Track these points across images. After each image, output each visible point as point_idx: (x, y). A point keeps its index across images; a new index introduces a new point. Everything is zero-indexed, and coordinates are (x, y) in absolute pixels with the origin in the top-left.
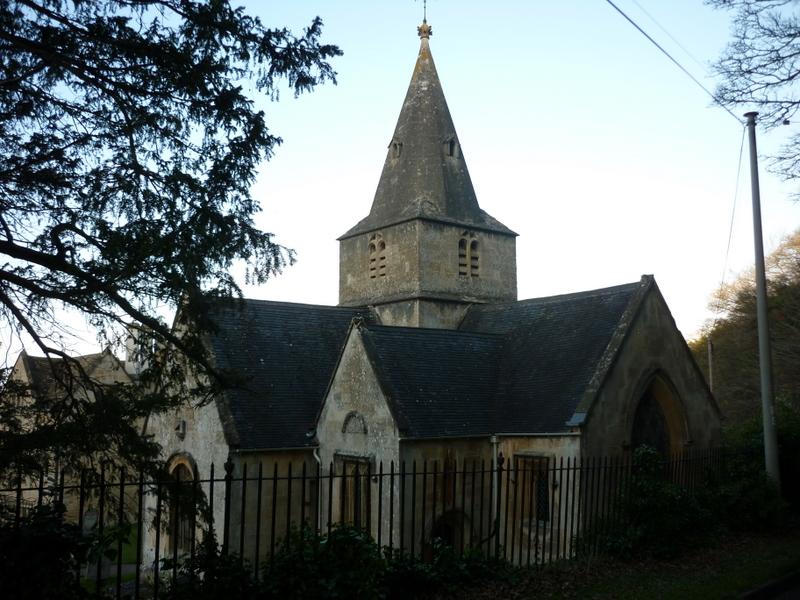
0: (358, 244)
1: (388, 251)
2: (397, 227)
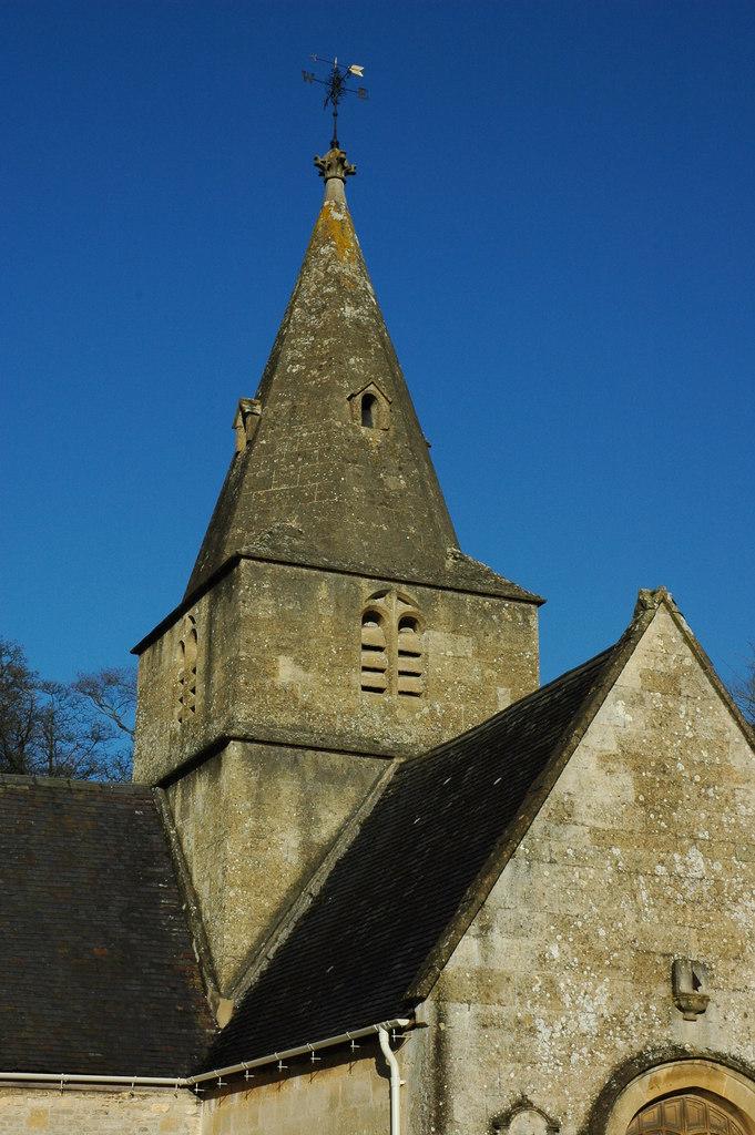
0: (323, 592)
1: (435, 641)
2: (469, 598)
